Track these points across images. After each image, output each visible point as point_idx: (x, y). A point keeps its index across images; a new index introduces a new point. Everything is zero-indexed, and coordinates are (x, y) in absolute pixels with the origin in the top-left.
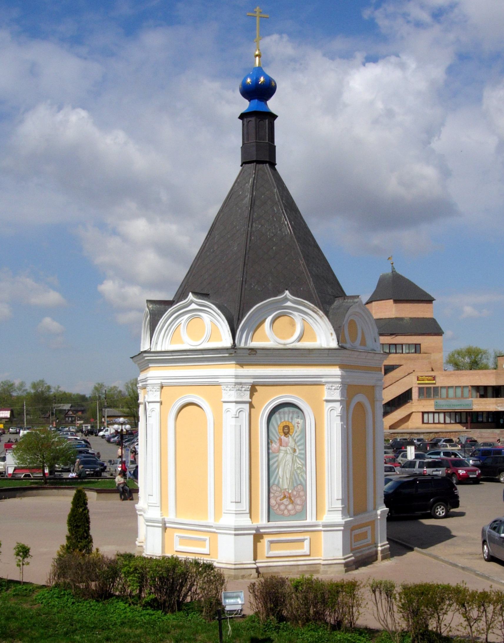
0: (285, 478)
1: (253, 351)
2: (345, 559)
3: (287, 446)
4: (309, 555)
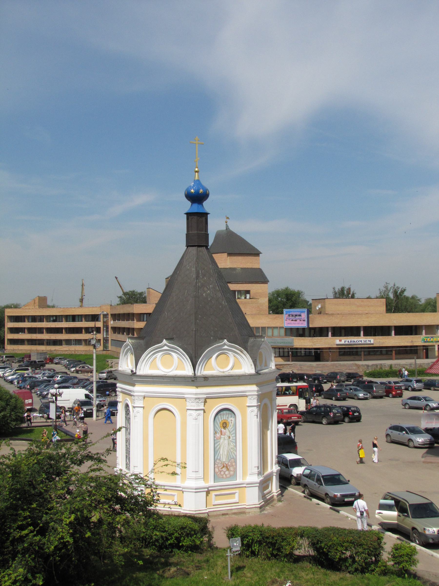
0: (224, 456)
1: (206, 378)
2: (259, 504)
3: (225, 435)
4: (238, 503)
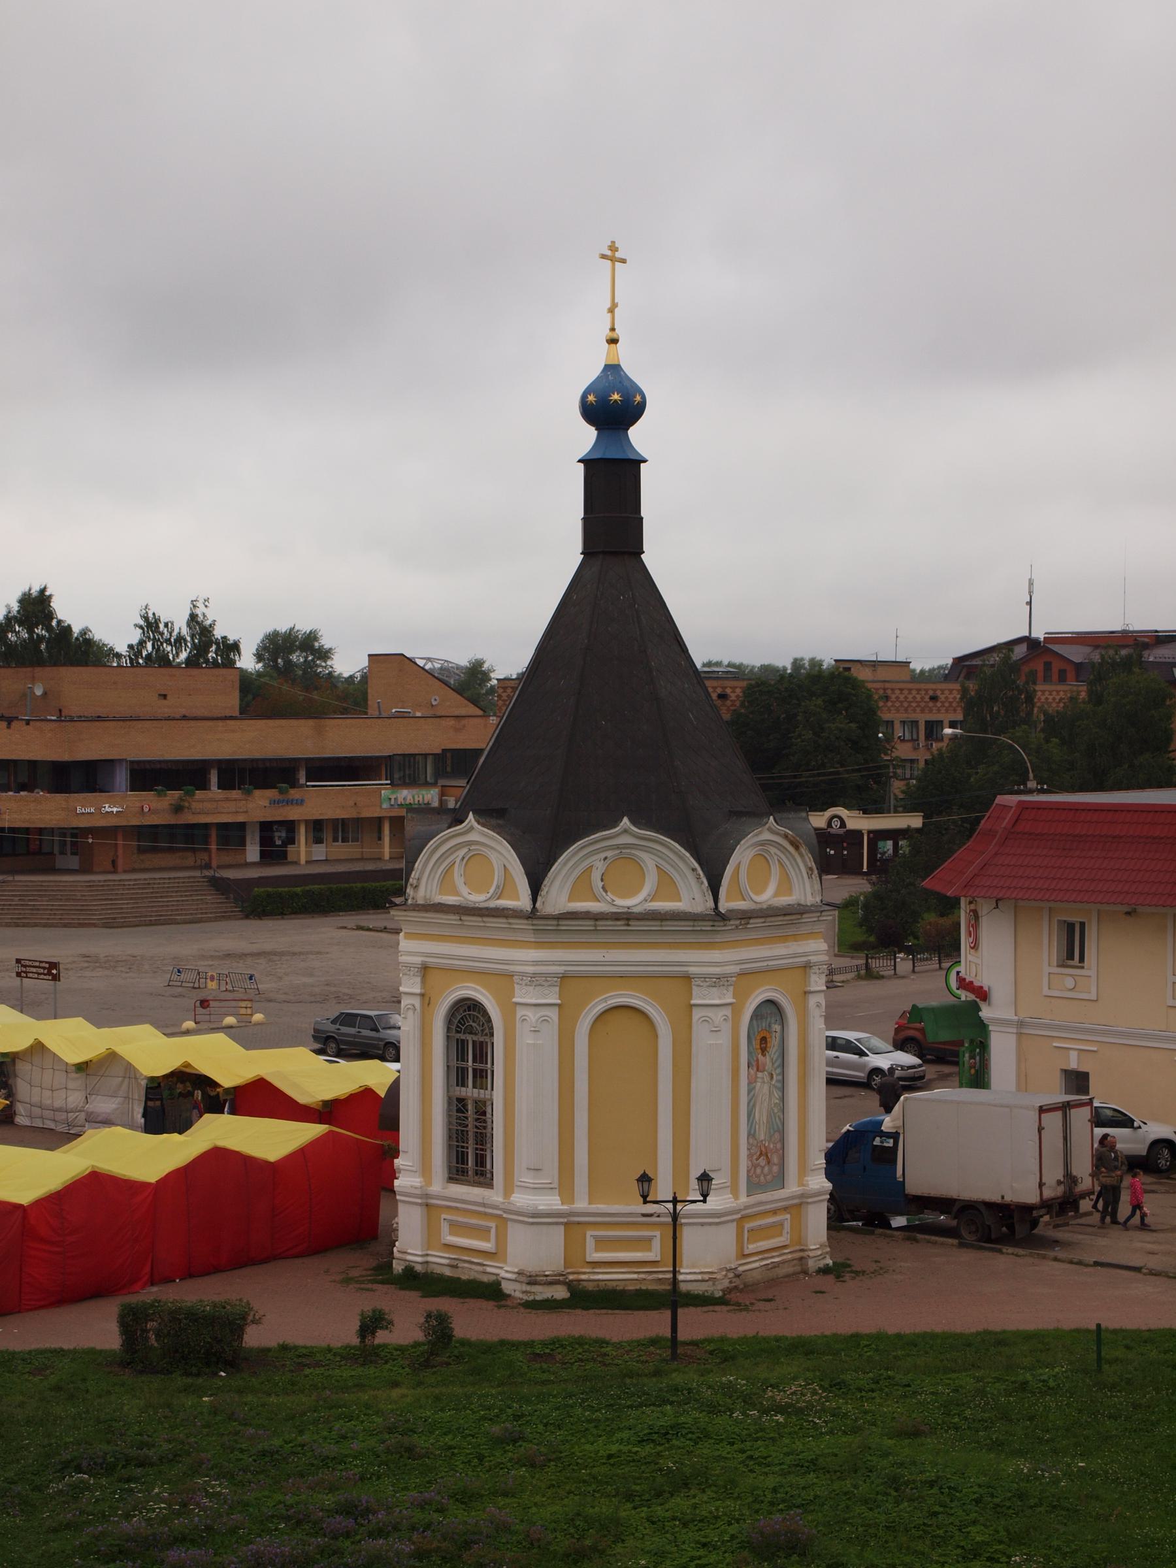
1: (745, 917)
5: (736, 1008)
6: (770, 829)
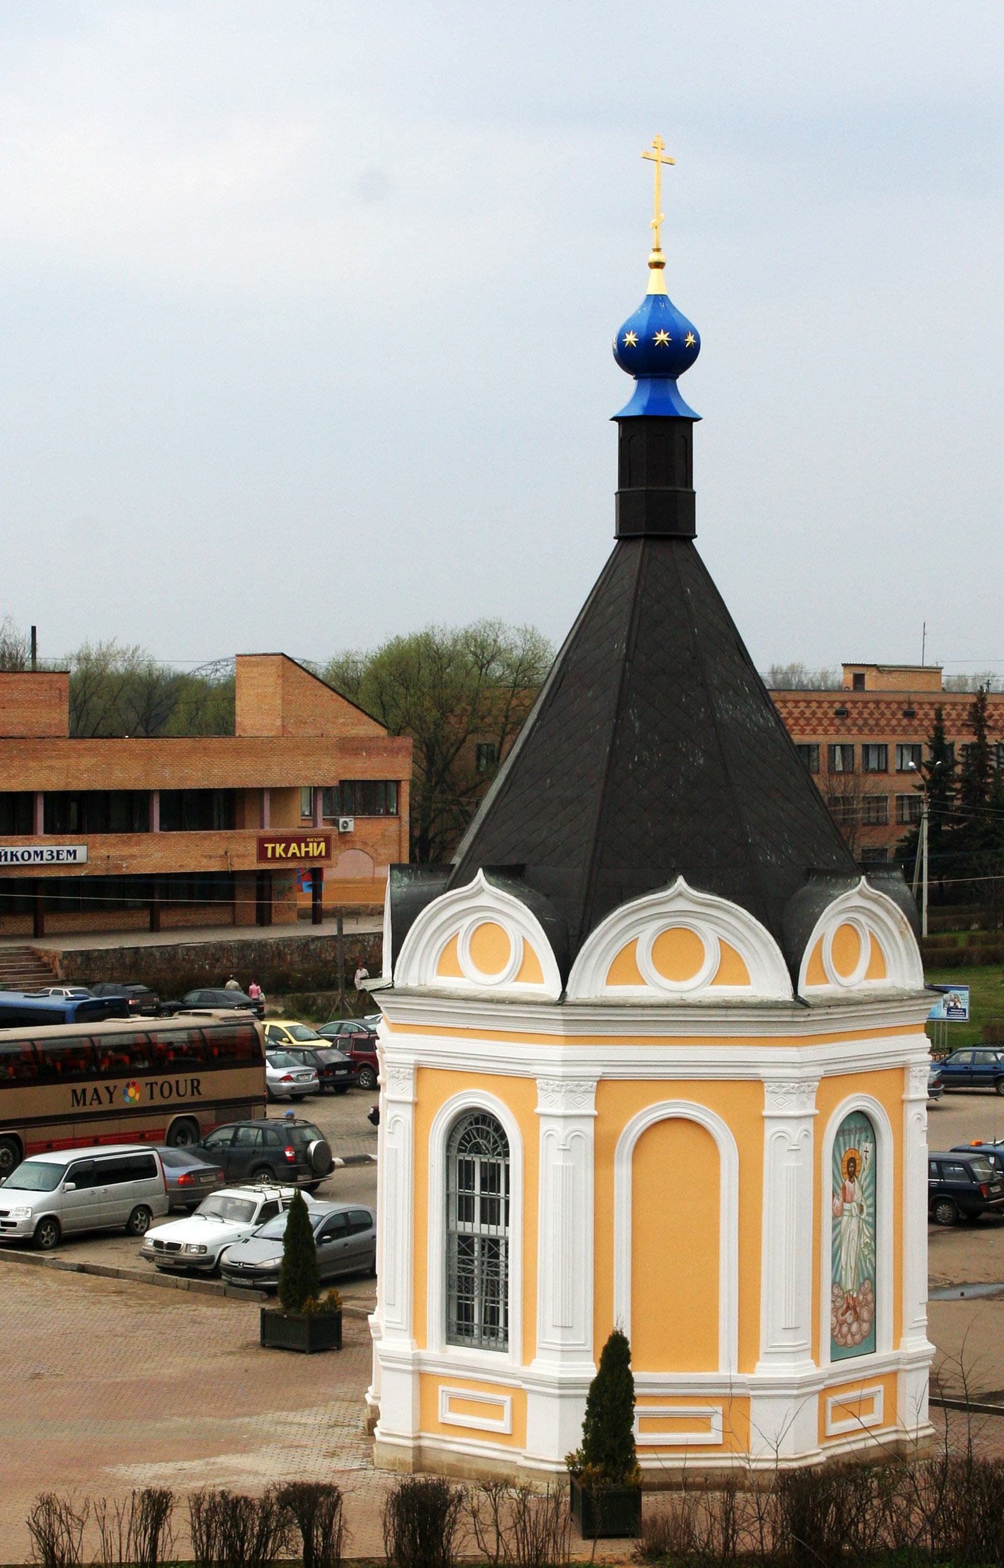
5: (819, 1122)
6: (860, 893)
